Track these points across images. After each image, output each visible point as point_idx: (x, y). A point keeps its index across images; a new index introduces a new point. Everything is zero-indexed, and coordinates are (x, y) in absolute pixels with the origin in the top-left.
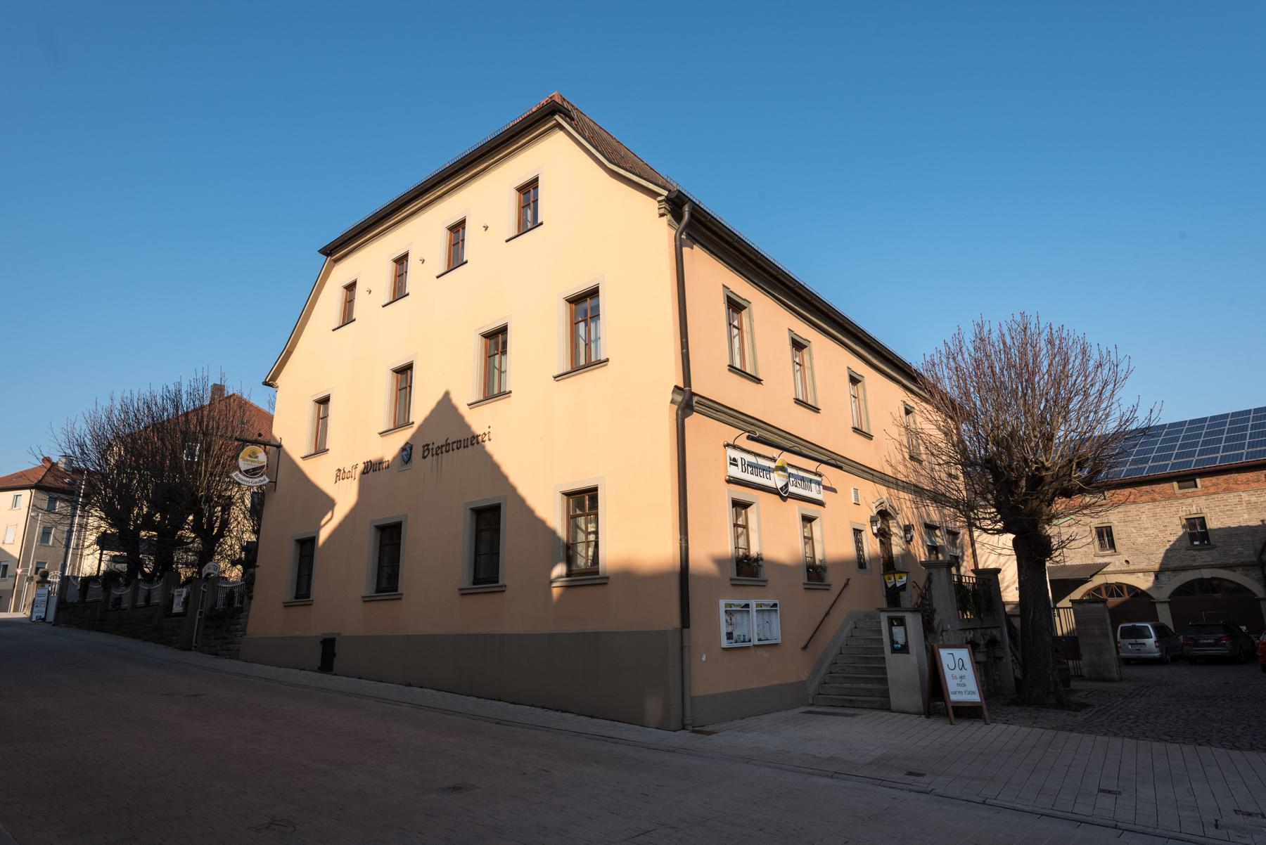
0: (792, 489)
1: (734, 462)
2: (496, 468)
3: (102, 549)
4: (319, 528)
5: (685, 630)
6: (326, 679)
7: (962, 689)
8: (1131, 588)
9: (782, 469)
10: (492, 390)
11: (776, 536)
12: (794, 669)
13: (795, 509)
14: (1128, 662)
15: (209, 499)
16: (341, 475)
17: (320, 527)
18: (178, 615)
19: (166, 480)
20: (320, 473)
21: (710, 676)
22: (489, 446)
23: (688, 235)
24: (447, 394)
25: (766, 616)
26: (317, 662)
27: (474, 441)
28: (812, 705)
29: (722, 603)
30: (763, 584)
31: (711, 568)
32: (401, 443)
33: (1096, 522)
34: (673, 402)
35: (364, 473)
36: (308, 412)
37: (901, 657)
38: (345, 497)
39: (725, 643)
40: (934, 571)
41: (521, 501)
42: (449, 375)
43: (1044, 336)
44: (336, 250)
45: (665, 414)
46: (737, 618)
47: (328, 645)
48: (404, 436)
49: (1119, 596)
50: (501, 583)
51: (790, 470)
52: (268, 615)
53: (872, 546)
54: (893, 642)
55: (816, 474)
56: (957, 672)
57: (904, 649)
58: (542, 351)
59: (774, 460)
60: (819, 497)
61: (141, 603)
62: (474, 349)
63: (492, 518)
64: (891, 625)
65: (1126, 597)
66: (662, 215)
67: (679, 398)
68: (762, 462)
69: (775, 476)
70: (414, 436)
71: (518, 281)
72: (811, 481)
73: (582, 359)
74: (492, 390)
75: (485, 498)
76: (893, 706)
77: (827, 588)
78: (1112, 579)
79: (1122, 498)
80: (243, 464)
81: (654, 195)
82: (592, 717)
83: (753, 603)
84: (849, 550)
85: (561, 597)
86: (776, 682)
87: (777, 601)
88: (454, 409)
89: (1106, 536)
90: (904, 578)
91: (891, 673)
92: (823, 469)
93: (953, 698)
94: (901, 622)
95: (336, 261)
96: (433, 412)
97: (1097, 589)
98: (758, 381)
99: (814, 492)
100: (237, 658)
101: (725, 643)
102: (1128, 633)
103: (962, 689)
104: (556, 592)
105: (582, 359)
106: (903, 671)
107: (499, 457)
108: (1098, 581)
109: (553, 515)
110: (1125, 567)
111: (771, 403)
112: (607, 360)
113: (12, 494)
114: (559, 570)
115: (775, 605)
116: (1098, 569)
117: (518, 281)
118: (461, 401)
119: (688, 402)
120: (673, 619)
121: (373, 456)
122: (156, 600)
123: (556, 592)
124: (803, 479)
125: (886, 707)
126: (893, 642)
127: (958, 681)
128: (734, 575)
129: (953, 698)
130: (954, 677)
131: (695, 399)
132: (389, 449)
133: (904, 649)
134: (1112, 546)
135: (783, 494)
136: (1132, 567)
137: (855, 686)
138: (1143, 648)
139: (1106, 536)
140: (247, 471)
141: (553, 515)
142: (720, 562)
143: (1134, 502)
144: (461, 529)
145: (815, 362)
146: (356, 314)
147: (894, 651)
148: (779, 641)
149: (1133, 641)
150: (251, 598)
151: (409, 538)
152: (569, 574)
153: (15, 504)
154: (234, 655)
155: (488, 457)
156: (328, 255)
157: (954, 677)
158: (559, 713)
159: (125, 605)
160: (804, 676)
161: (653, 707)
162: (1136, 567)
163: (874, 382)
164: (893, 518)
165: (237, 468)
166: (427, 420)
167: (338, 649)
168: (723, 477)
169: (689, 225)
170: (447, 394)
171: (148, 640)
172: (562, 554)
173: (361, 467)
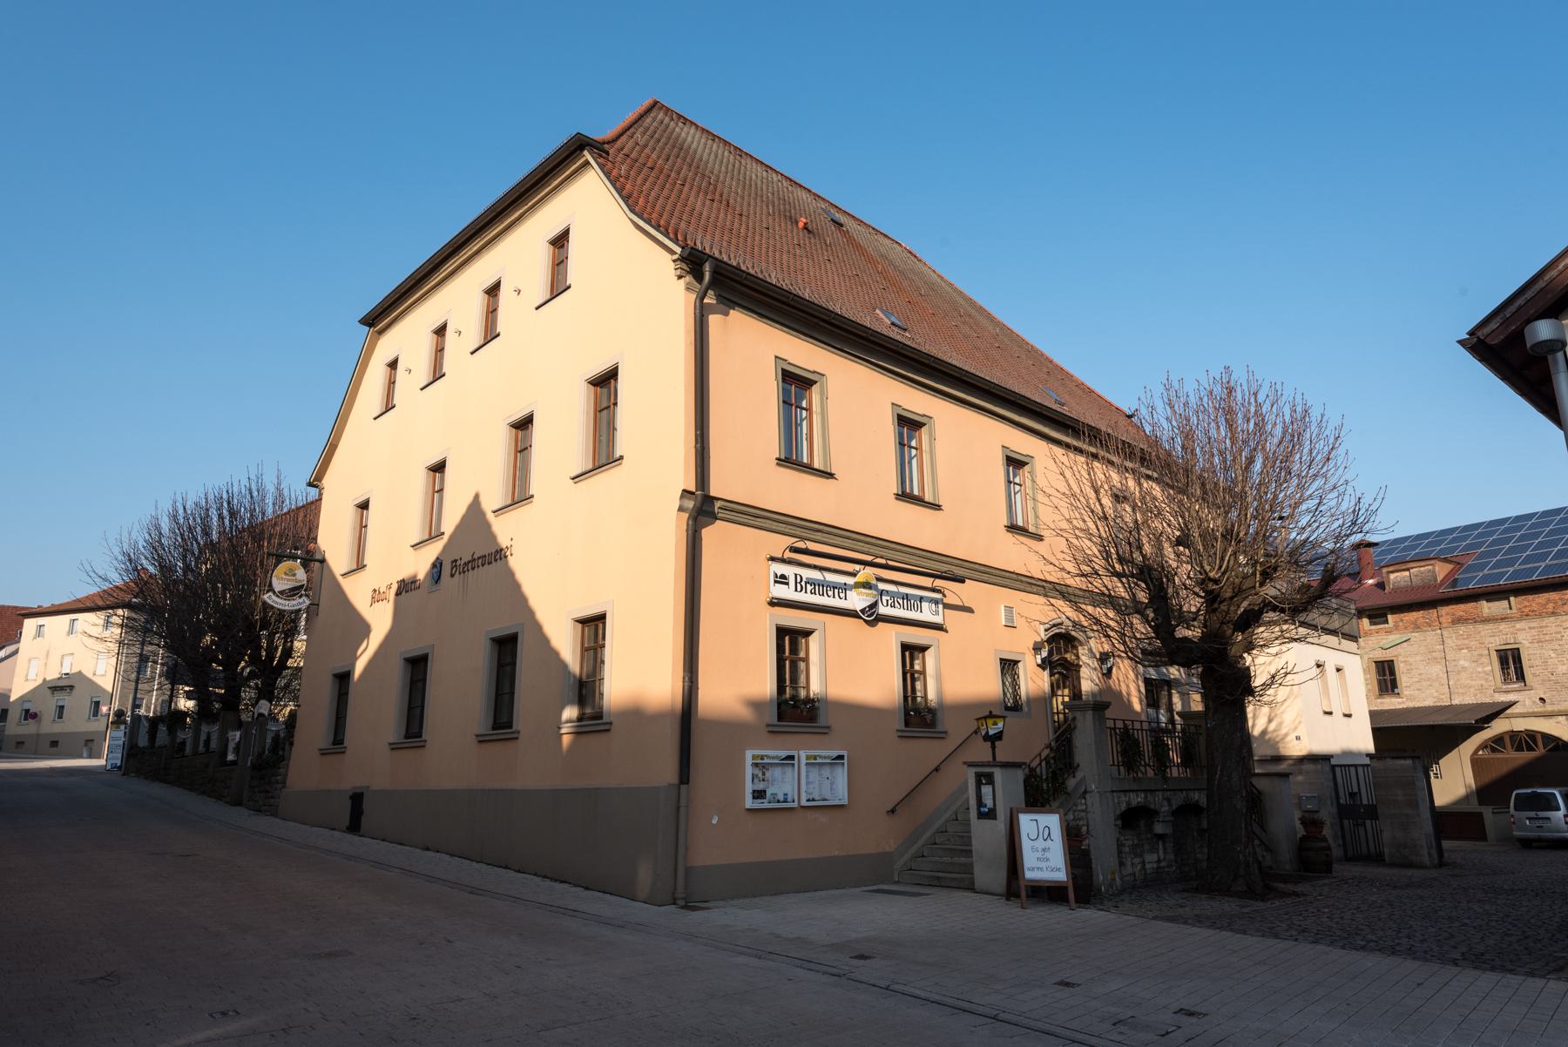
0: (883, 610)
2: (516, 586)
3: (173, 684)
4: (353, 665)
5: (683, 787)
7: (1043, 865)
8: (1547, 738)
9: (867, 585)
10: (519, 495)
11: (854, 669)
12: (878, 837)
13: (890, 639)
14: (1527, 844)
15: (265, 624)
16: (377, 596)
17: (356, 659)
19: (217, 601)
20: (358, 591)
21: (715, 841)
22: (513, 562)
23: (719, 297)
24: (477, 496)
25: (826, 772)
27: (499, 555)
28: (897, 883)
29: (749, 754)
30: (826, 730)
31: (745, 713)
32: (432, 559)
33: (1497, 642)
34: (681, 509)
35: (398, 594)
36: (349, 514)
37: (987, 823)
38: (380, 620)
39: (749, 803)
40: (1078, 715)
41: (538, 628)
42: (479, 476)
43: (1183, 400)
44: (380, 317)
45: (670, 528)
46: (775, 773)
47: (357, 799)
48: (433, 551)
49: (1530, 749)
50: (940, 728)
51: (882, 586)
52: (306, 769)
53: (1034, 680)
54: (980, 803)
55: (933, 590)
56: (1040, 844)
57: (992, 814)
58: (544, 446)
59: (854, 575)
60: (938, 619)
61: (201, 748)
62: (502, 438)
63: (508, 649)
64: (979, 785)
65: (1540, 751)
66: (680, 277)
67: (690, 504)
68: (830, 577)
69: (852, 594)
70: (445, 547)
71: (541, 361)
72: (921, 599)
73: (604, 455)
74: (519, 495)
75: (502, 628)
77: (942, 735)
78: (1520, 725)
79: (1535, 607)
80: (279, 583)
81: (672, 252)
82: (587, 889)
83: (803, 754)
84: (989, 686)
85: (573, 745)
87: (844, 753)
88: (483, 514)
89: (1511, 661)
90: (1000, 725)
91: (976, 845)
92: (939, 583)
93: (1029, 875)
94: (990, 779)
95: (381, 332)
96: (464, 518)
97: (1499, 740)
98: (830, 475)
99: (927, 613)
101: (749, 803)
102: (1526, 803)
103: (1043, 865)
104: (566, 740)
105: (604, 455)
107: (520, 576)
108: (1499, 727)
109: (565, 643)
110: (1539, 708)
111: (858, 496)
112: (621, 458)
113: (67, 618)
114: (570, 713)
115: (841, 757)
116: (1499, 711)
117: (541, 361)
118: (489, 505)
119: (703, 508)
120: (665, 771)
121: (405, 573)
122: (214, 745)
123: (566, 740)
124: (906, 597)
125: (971, 887)
126: (980, 803)
127: (1039, 855)
128: (774, 720)
129: (1029, 875)
130: (1034, 849)
131: (718, 504)
132: (419, 565)
134: (1521, 676)
135: (872, 617)
136: (1549, 708)
137: (956, 860)
138: (1546, 825)
139: (1511, 661)
140: (282, 592)
141: (565, 643)
142: (756, 705)
143: (1554, 614)
145: (939, 445)
147: (981, 816)
148: (845, 802)
149: (1532, 814)
150: (292, 744)
151: (435, 671)
152: (580, 719)
153: (71, 631)
154: (273, 812)
155: (511, 574)
156: (370, 325)
157: (1034, 849)
158: (548, 882)
159: (188, 750)
160: (890, 846)
161: (644, 875)
162: (1556, 708)
163: (1049, 462)
164: (1081, 644)
165: (271, 589)
166: (459, 528)
168: (765, 599)
169: (714, 284)
170: (477, 496)
171: (203, 793)
172: (574, 694)
173: (395, 587)
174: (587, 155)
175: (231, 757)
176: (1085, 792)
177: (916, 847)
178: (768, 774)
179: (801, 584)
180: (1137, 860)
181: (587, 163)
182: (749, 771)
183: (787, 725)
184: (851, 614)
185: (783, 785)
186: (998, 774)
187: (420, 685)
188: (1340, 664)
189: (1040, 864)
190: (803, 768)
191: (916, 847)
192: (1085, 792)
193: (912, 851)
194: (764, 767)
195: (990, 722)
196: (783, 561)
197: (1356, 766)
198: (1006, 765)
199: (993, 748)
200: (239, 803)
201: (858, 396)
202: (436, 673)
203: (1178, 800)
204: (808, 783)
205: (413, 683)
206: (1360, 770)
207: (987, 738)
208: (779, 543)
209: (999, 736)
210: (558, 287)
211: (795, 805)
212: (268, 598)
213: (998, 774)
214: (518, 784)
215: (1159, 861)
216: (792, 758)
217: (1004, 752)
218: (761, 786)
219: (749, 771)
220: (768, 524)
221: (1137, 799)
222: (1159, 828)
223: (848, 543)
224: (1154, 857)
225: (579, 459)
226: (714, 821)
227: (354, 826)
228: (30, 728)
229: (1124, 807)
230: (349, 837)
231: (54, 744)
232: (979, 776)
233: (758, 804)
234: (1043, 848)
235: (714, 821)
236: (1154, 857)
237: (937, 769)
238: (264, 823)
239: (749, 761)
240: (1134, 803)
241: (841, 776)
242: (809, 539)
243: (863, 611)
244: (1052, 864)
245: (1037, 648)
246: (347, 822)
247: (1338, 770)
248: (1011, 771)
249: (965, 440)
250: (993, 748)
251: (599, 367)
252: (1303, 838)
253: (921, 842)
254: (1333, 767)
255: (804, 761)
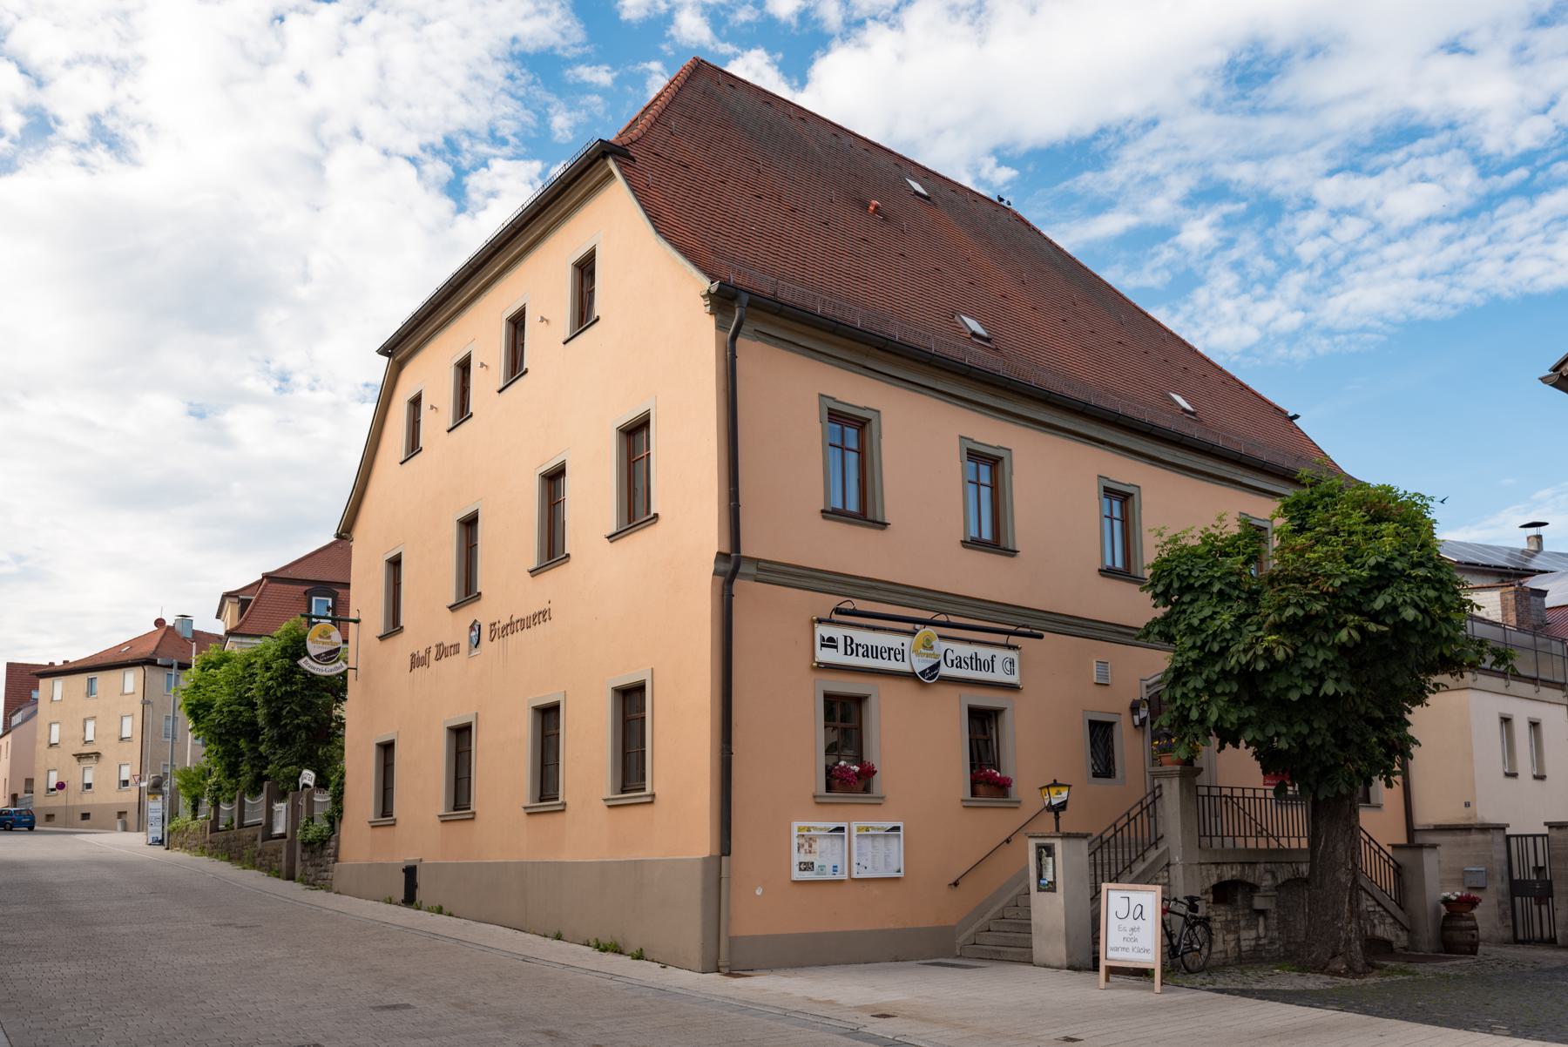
1: (830, 643)
6: (406, 915)
18: (283, 836)
25: (880, 843)
26: (401, 896)
29: (795, 825)
30: (879, 801)
39: (797, 875)
40: (1165, 782)
47: (410, 872)
52: (357, 838)
54: (1040, 876)
57: (1052, 887)
62: (451, 533)
64: (1039, 859)
73: (635, 509)
76: (1035, 959)
80: (314, 648)
82: (603, 948)
83: (854, 826)
86: (892, 926)
92: (1013, 640)
94: (1049, 850)
100: (329, 890)
103: (1130, 945)
105: (635, 509)
106: (1050, 914)
112: (656, 515)
115: (897, 829)
119: (732, 566)
125: (1031, 963)
127: (1126, 935)
129: (1111, 954)
133: (1052, 887)
140: (318, 656)
144: (523, 729)
146: (598, 309)
165: (307, 654)
167: (421, 878)
174: (612, 165)
175: (279, 829)
176: (1168, 865)
177: (981, 921)
178: (816, 846)
179: (851, 647)
180: (1230, 937)
181: (610, 175)
182: (795, 842)
183: (836, 796)
184: (911, 676)
185: (828, 857)
186: (1058, 845)
187: (553, 739)
188: (1507, 711)
189: (1125, 944)
190: (854, 839)
191: (981, 921)
192: (1168, 865)
193: (977, 925)
194: (811, 839)
195: (1053, 791)
196: (830, 622)
197: (1535, 836)
198: (1067, 836)
199: (1057, 818)
200: (291, 877)
201: (923, 437)
202: (481, 744)
203: (1284, 874)
204: (859, 855)
205: (458, 753)
206: (1539, 840)
207: (1050, 808)
208: (826, 603)
209: (1063, 806)
210: (584, 316)
211: (845, 877)
212: (304, 663)
213: (1058, 845)
214: (566, 857)
215: (1258, 938)
216: (842, 829)
217: (1068, 821)
218: (808, 859)
219: (795, 842)
220: (815, 583)
221: (1229, 873)
222: (1259, 903)
223: (907, 599)
224: (1253, 934)
225: (530, 554)
226: (759, 892)
227: (410, 899)
228: (59, 799)
229: (1214, 881)
230: (404, 910)
231: (85, 816)
232: (1039, 847)
233: (807, 875)
234: (1133, 922)
235: (759, 892)
236: (1253, 934)
237: (1008, 841)
238: (319, 897)
239: (795, 833)
240: (1227, 877)
241: (896, 848)
242: (859, 598)
243: (923, 673)
244: (1139, 945)
245: (1135, 708)
246: (402, 896)
247: (1513, 840)
248: (1073, 843)
249: (1056, 479)
250: (1057, 818)
251: (628, 415)
252: (1446, 918)
253: (988, 916)
254: (1508, 838)
255: (855, 833)
